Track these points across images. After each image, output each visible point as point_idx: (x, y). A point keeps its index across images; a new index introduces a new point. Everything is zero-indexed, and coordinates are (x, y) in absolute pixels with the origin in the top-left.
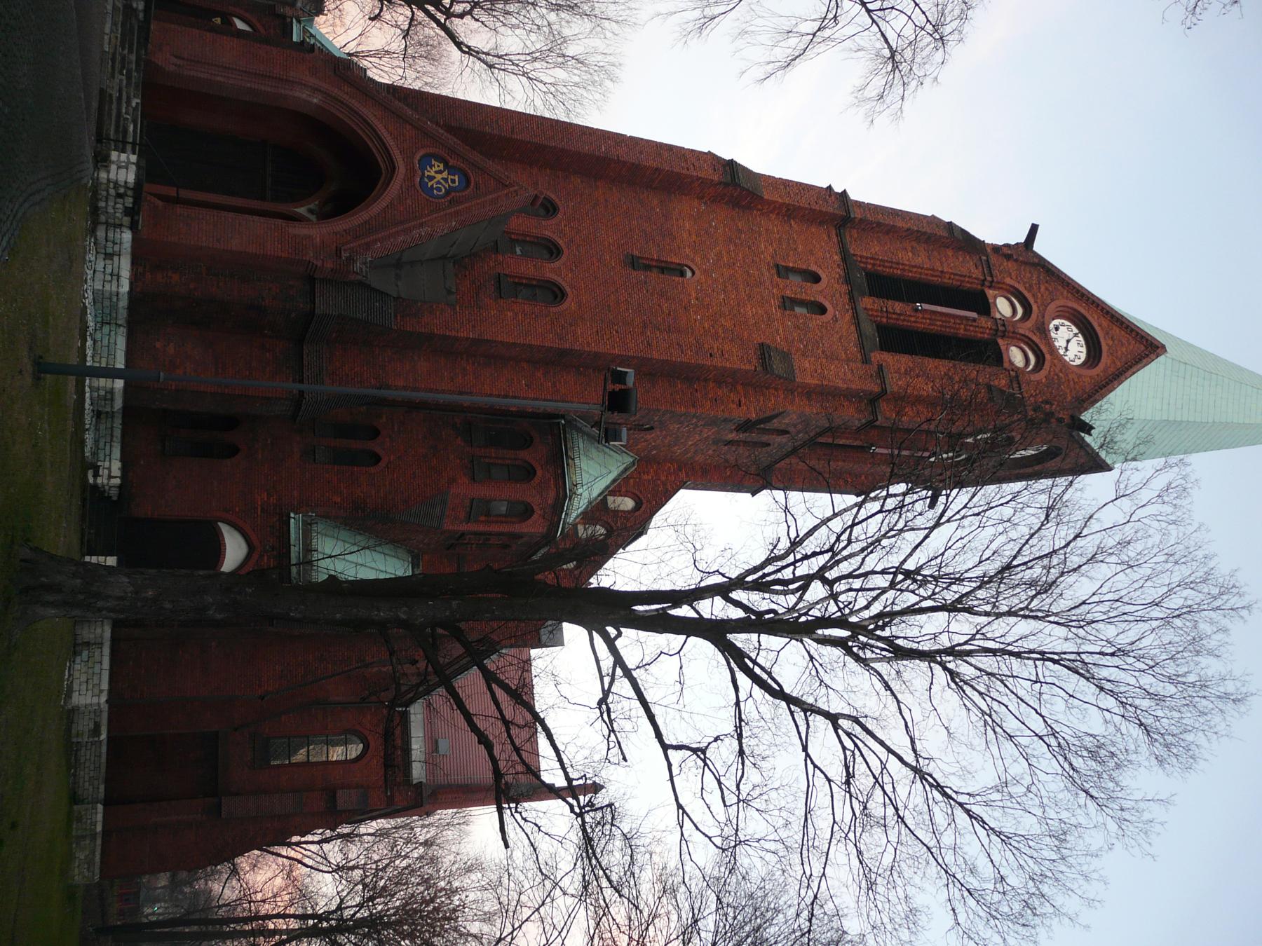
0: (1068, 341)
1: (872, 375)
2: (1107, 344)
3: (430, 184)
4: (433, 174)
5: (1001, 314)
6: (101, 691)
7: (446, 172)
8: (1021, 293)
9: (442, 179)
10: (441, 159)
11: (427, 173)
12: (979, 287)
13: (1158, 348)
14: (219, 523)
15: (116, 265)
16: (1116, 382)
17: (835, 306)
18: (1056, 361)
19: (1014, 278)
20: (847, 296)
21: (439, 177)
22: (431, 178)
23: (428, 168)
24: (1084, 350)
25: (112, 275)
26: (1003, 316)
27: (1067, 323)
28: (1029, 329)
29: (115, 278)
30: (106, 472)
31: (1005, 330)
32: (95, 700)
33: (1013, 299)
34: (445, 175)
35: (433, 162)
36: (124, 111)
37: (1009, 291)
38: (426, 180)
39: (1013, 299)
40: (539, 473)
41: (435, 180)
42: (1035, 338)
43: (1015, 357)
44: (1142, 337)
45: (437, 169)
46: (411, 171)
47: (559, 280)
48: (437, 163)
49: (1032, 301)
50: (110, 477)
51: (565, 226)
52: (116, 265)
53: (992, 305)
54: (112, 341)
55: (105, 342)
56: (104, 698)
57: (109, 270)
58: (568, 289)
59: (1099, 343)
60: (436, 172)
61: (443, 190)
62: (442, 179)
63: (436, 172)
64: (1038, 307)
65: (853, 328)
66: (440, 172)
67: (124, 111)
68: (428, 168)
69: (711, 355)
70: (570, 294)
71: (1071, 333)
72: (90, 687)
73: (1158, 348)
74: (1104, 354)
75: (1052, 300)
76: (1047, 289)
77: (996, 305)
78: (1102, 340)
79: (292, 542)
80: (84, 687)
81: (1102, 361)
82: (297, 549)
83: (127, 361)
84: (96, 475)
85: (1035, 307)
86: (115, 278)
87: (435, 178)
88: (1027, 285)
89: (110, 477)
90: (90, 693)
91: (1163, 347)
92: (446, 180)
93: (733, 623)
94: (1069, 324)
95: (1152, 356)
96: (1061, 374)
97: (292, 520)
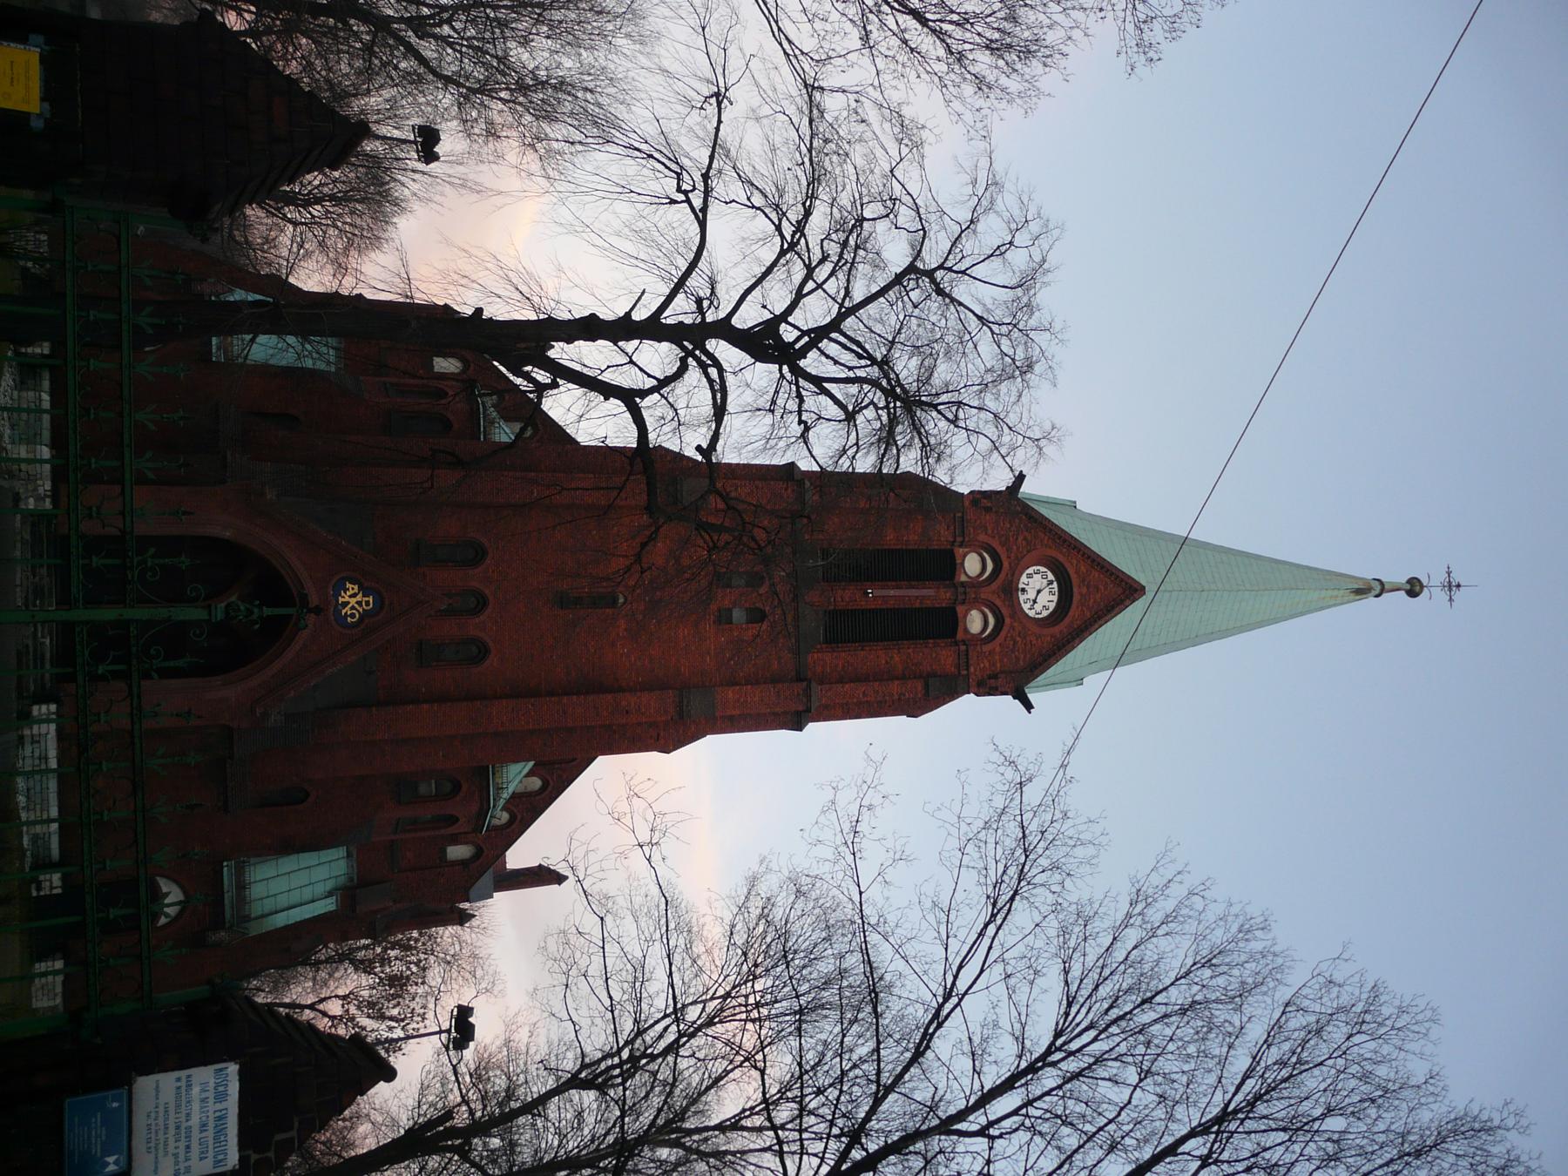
0: (1039, 592)
1: (798, 694)
2: (1081, 594)
3: (344, 612)
4: (347, 599)
6: (56, 995)
7: (361, 595)
9: (357, 603)
11: (341, 600)
12: (949, 547)
13: (1136, 590)
14: (158, 878)
15: (43, 748)
18: (1015, 624)
19: (990, 532)
21: (353, 601)
22: (346, 604)
23: (343, 594)
24: (1055, 598)
25: (40, 759)
27: (1043, 569)
28: (994, 592)
29: (43, 761)
30: (48, 883)
31: (973, 593)
32: (51, 1003)
33: (985, 554)
34: (359, 598)
35: (348, 585)
36: (40, 635)
38: (340, 607)
39: (985, 554)
40: (465, 787)
41: (350, 606)
42: (998, 602)
43: (973, 621)
44: (1122, 580)
45: (351, 592)
48: (351, 586)
49: (1004, 557)
50: (52, 888)
51: (493, 572)
52: (43, 748)
53: (958, 566)
54: (44, 786)
55: (38, 788)
56: (59, 1000)
57: (37, 754)
58: (491, 644)
59: (1072, 596)
60: (350, 596)
61: (357, 616)
62: (357, 603)
63: (350, 596)
64: (1010, 564)
66: (354, 596)
67: (40, 635)
68: (343, 594)
69: (627, 712)
71: (1045, 581)
72: (46, 992)
73: (1136, 590)
76: (1025, 539)
77: (962, 564)
78: (1075, 590)
79: (226, 886)
80: (40, 993)
81: (1070, 613)
82: (230, 894)
83: (60, 812)
84: (39, 889)
85: (1006, 564)
86: (43, 761)
87: (349, 603)
88: (1003, 539)
89: (52, 888)
90: (45, 998)
91: (1143, 588)
92: (359, 603)
94: (1046, 570)
95: (1127, 602)
96: (1018, 639)
97: (225, 869)
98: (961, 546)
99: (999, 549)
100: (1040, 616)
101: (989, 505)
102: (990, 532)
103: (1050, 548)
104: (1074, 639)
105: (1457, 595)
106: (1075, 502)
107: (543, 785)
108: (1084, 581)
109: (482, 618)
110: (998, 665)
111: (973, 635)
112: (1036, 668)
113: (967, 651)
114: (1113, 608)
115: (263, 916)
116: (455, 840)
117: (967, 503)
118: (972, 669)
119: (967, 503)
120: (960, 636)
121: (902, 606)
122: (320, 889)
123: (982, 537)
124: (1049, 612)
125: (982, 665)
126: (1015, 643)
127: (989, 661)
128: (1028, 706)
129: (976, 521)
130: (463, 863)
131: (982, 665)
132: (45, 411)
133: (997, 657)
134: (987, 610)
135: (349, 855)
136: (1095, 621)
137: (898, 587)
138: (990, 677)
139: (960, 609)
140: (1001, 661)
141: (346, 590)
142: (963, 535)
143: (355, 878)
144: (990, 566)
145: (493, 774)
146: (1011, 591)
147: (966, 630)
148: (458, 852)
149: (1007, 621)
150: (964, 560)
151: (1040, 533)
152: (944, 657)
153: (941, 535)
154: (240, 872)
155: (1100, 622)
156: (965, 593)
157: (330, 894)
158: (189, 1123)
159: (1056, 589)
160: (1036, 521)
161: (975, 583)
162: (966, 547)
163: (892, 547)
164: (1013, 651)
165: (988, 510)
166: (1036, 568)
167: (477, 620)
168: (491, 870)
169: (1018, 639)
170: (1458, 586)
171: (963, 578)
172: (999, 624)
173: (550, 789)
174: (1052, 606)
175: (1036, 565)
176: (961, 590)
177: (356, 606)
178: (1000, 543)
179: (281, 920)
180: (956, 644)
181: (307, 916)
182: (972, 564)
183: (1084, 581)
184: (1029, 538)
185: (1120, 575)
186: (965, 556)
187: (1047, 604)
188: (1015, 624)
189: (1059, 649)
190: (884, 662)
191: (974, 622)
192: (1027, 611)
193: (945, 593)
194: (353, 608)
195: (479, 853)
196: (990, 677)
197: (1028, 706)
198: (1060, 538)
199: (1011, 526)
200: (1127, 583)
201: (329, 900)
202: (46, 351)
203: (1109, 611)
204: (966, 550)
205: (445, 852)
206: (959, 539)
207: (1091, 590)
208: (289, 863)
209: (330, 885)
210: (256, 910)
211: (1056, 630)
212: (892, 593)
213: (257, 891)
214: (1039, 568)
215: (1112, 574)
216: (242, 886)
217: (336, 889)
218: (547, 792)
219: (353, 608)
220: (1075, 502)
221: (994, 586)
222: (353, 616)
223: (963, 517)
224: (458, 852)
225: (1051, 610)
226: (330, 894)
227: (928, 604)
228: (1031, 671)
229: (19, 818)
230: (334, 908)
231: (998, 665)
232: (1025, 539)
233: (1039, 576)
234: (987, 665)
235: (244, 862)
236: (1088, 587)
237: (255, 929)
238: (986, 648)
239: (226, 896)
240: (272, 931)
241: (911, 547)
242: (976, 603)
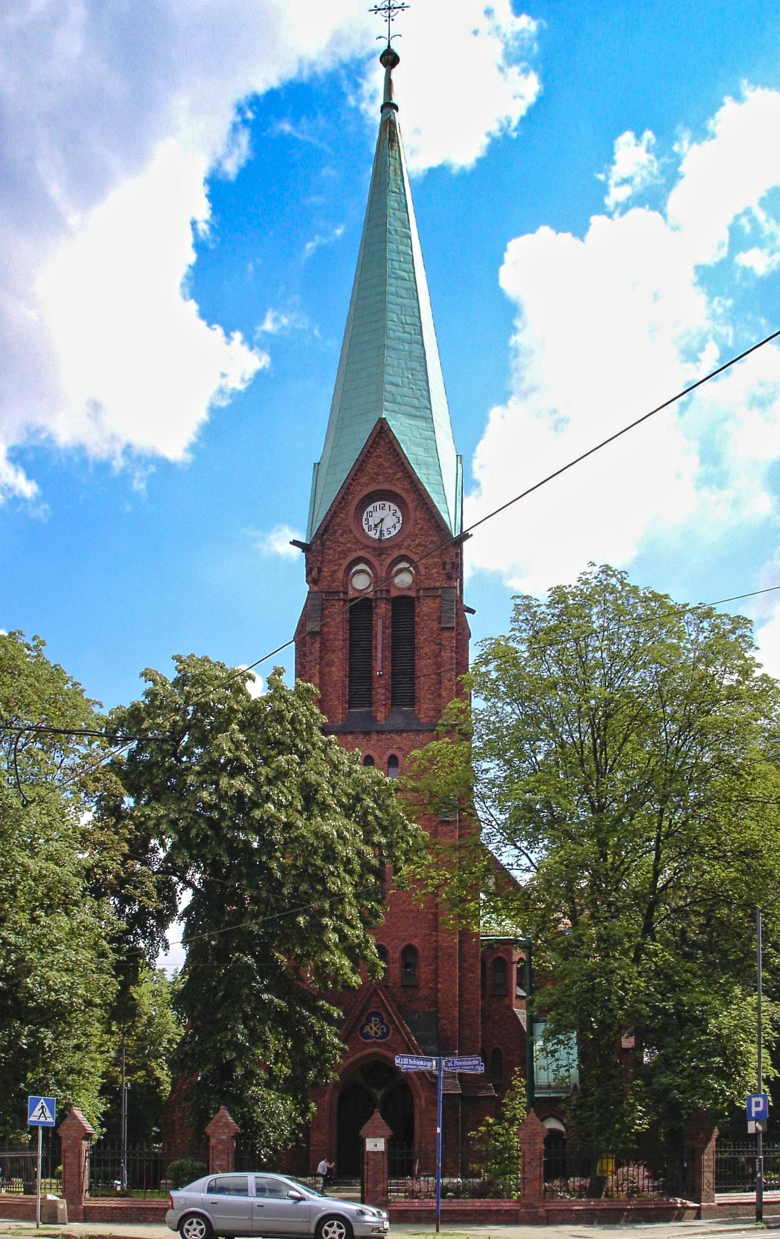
4: (373, 1032)
5: (368, 588)
8: (349, 564)
10: (363, 1028)
16: (427, 500)
17: (389, 747)
18: (406, 544)
19: (336, 568)
20: (380, 735)
21: (374, 1028)
22: (376, 1033)
24: (388, 504)
26: (370, 583)
27: (365, 516)
28: (381, 564)
31: (382, 582)
33: (353, 571)
35: (365, 1031)
37: (348, 574)
39: (353, 571)
42: (389, 561)
45: (369, 1029)
46: (375, 1044)
47: (400, 949)
58: (406, 943)
59: (386, 490)
65: (405, 735)
66: (371, 1028)
70: (409, 942)
74: (393, 488)
75: (351, 532)
85: (361, 553)
92: (375, 1025)
93: (308, 608)
95: (391, 437)
98: (347, 593)
100: (401, 518)
101: (316, 569)
102: (336, 568)
103: (348, 512)
104: (418, 490)
106: (315, 464)
108: (374, 479)
109: (389, 948)
110: (436, 560)
111: (413, 581)
112: (439, 526)
113: (424, 589)
114: (395, 450)
117: (316, 588)
118: (438, 584)
119: (316, 588)
120: (412, 594)
121: (390, 644)
123: (340, 575)
127: (433, 568)
129: (328, 581)
131: (435, 575)
132: (760, 1196)
134: (395, 569)
136: (405, 468)
137: (376, 648)
138: (444, 568)
139: (394, 593)
141: (368, 1032)
142: (339, 592)
144: (362, 566)
146: (380, 548)
147: (409, 588)
149: (403, 552)
151: (337, 521)
152: (426, 607)
153: (338, 612)
155: (406, 464)
156: (381, 591)
158: (252, 1189)
159: (380, 503)
160: (327, 526)
161: (375, 580)
162: (347, 588)
163: (348, 651)
164: (426, 547)
165: (320, 571)
167: (390, 952)
169: (417, 542)
172: (403, 558)
174: (394, 507)
176: (379, 595)
178: (345, 558)
180: (418, 598)
182: (361, 582)
183: (374, 479)
184: (341, 531)
185: (369, 444)
186: (354, 589)
189: (425, 504)
190: (429, 661)
191: (404, 580)
193: (381, 609)
194: (378, 1029)
196: (444, 568)
198: (340, 503)
199: (331, 548)
200: (376, 437)
203: (398, 455)
204: (350, 588)
206: (342, 595)
207: (381, 472)
211: (411, 506)
212: (380, 655)
214: (364, 520)
215: (369, 452)
219: (378, 1029)
220: (315, 464)
221: (377, 564)
222: (383, 1029)
223: (326, 593)
225: (396, 508)
227: (388, 622)
228: (442, 530)
231: (436, 560)
232: (342, 535)
233: (370, 519)
234: (435, 570)
236: (378, 475)
241: (348, 636)
242: (389, 578)
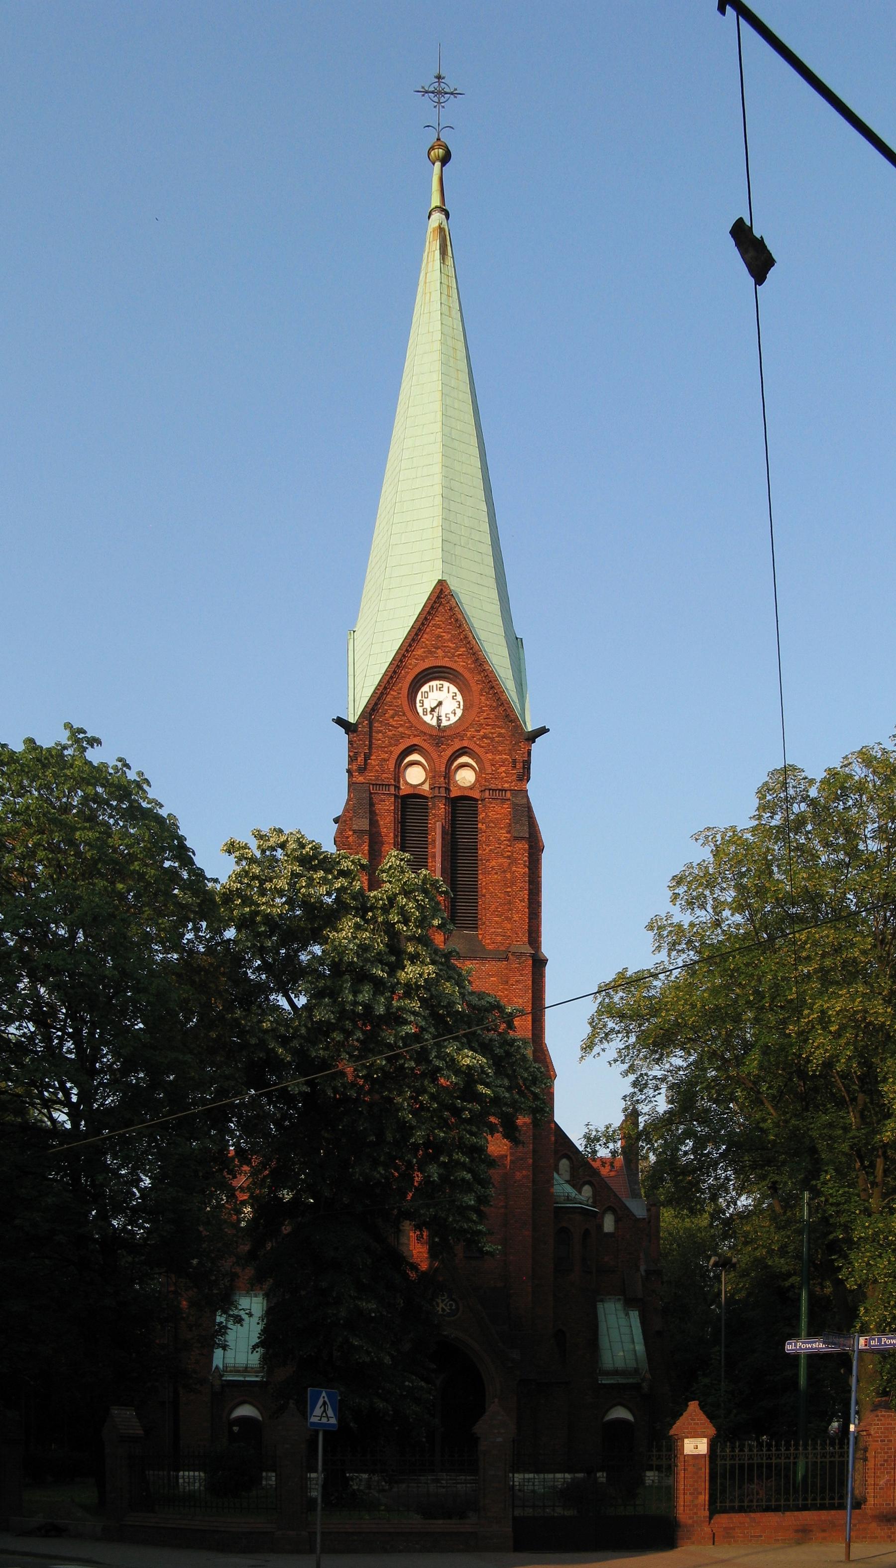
11: (440, 1312)
22: (443, 1310)
24: (446, 684)
34: (440, 1301)
39: (406, 761)
64: (415, 736)
77: (414, 787)
94: (420, 694)
96: (481, 733)
99: (402, 747)
100: (462, 704)
105: (451, 83)
107: (564, 1157)
108: (430, 652)
111: (477, 780)
115: (636, 1360)
116: (600, 1227)
118: (506, 786)
120: (476, 795)
122: (623, 1321)
124: (458, 693)
125: (504, 774)
126: (485, 737)
128: (543, 731)
130: (617, 1221)
131: (504, 774)
133: (498, 757)
134: (456, 764)
135: (602, 1301)
140: (500, 753)
143: (617, 1297)
145: (557, 1203)
147: (471, 788)
148: (608, 1224)
150: (411, 785)
154: (608, 1373)
157: (627, 1314)
161: (432, 774)
162: (399, 782)
164: (492, 739)
166: (418, 705)
168: (624, 1199)
170: (439, 77)
171: (426, 787)
173: (569, 1153)
175: (415, 703)
177: (445, 1302)
179: (640, 1347)
181: (640, 1331)
183: (430, 652)
187: (451, 694)
188: (469, 734)
191: (466, 777)
192: (457, 718)
194: (446, 1305)
195: (611, 1209)
197: (543, 731)
200: (435, 602)
201: (631, 1313)
202: (274, 1474)
205: (607, 1234)
208: (604, 1342)
209: (621, 1314)
210: (632, 1364)
213: (620, 1364)
214: (418, 701)
216: (616, 1372)
217: (625, 1309)
218: (572, 1156)
221: (434, 755)
222: (451, 1305)
224: (608, 1224)
226: (627, 1314)
229: (261, 1484)
230: (637, 1312)
232: (393, 717)
233: (425, 700)
234: (503, 769)
235: (600, 1371)
237: (644, 1366)
238: (487, 765)
239: (620, 1382)
240: (647, 1355)
242: (448, 775)
